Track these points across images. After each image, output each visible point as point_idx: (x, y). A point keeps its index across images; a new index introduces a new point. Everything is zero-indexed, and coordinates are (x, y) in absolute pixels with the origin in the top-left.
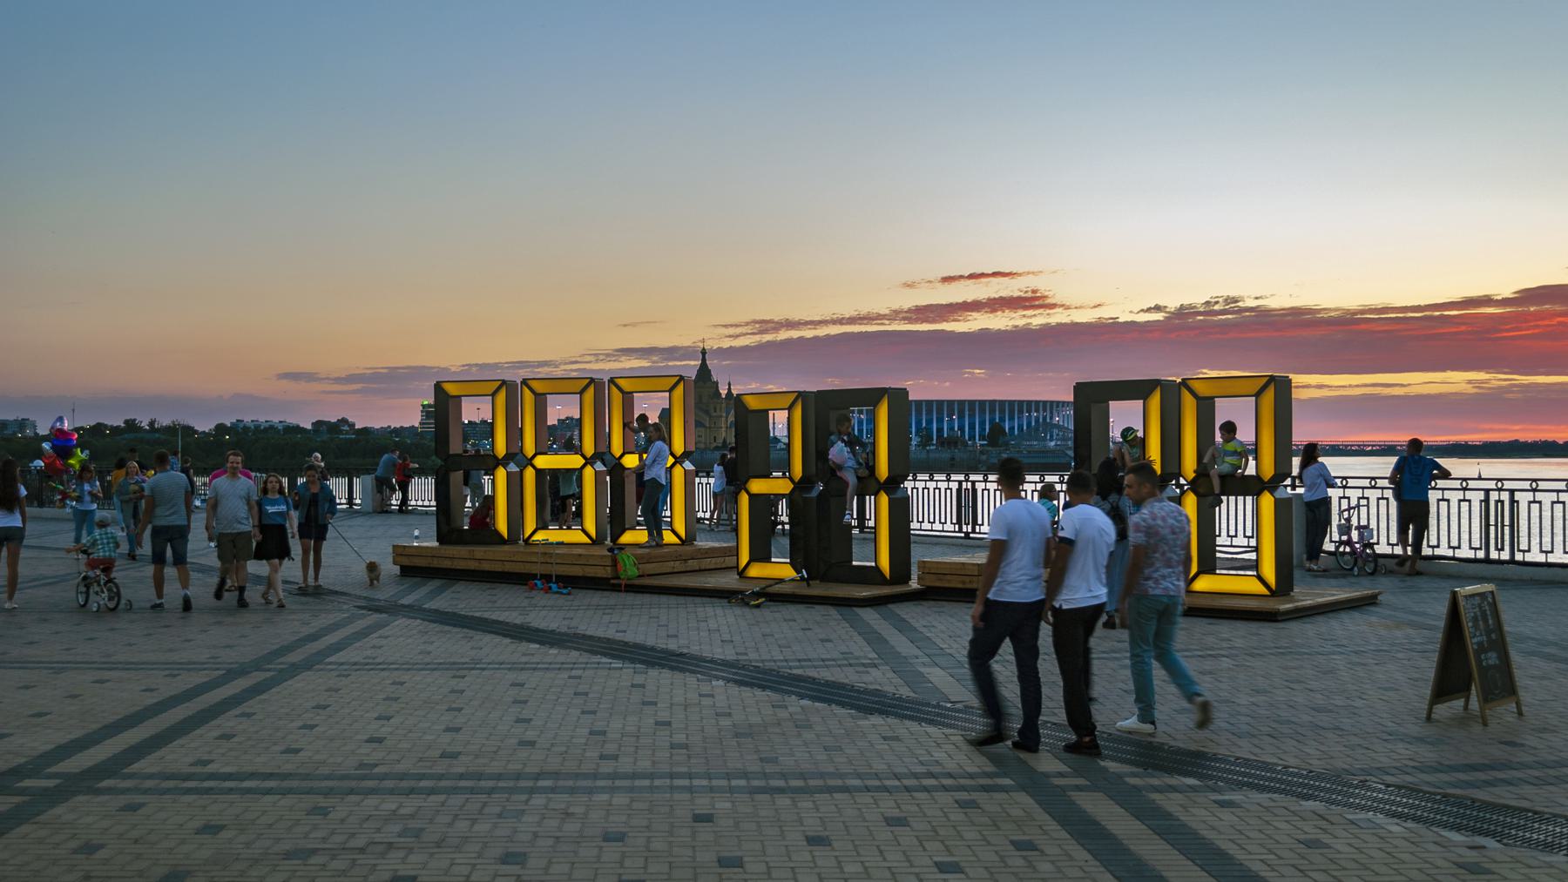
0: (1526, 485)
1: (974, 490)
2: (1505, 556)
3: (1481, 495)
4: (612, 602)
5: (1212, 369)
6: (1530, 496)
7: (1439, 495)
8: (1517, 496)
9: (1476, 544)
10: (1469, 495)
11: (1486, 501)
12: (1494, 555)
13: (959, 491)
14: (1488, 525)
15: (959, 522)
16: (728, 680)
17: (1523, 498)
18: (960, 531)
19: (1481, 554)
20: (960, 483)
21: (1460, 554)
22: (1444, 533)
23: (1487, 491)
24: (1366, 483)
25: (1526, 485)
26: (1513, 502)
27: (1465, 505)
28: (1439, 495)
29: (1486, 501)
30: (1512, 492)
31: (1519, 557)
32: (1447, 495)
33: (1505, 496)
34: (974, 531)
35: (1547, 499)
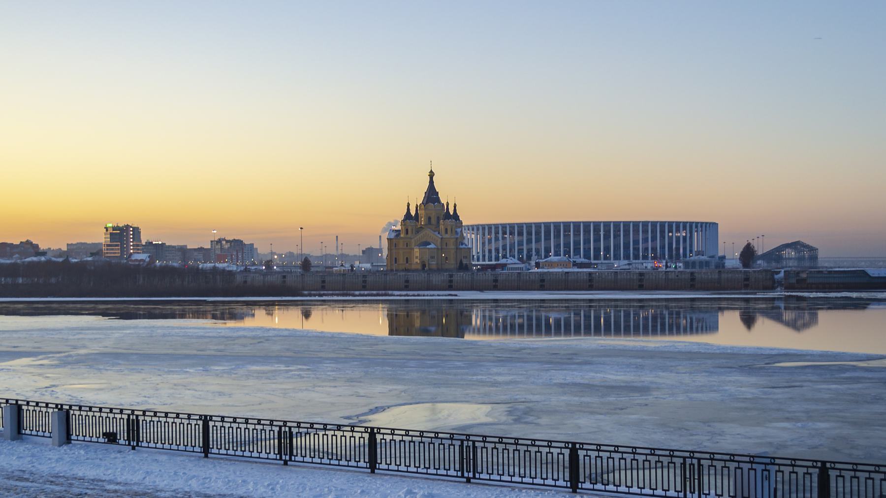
0: (707, 456)
3: (681, 460)
5: (33, 262)
9: (679, 489)
10: (674, 460)
11: (684, 464)
13: (128, 420)
14: (463, 459)
15: (280, 453)
18: (281, 459)
20: (129, 415)
21: (669, 494)
23: (684, 458)
24: (563, 445)
25: (707, 456)
27: (752, 472)
28: (584, 452)
29: (684, 464)
30: (699, 459)
32: (741, 465)
34: (290, 460)
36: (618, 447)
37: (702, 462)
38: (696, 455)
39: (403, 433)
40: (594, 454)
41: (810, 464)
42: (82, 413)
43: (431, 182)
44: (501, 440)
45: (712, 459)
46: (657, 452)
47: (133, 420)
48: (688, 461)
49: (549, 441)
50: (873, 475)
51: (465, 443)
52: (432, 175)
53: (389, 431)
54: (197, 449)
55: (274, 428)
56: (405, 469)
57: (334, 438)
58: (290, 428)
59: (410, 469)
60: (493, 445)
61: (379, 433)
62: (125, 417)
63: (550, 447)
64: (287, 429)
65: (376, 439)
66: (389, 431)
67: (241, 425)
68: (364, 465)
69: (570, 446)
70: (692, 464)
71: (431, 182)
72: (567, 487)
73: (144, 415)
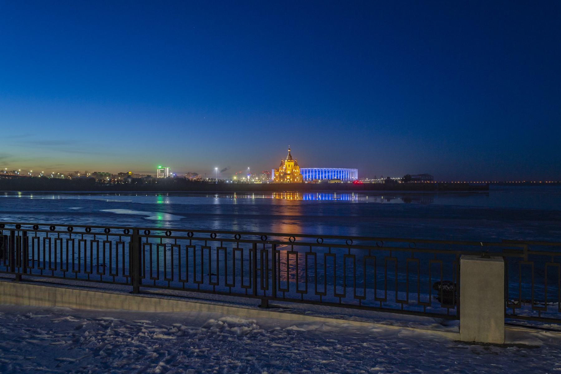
20: (13, 232)
39: (83, 230)
47: (19, 238)
64: (21, 234)
72: (127, 284)
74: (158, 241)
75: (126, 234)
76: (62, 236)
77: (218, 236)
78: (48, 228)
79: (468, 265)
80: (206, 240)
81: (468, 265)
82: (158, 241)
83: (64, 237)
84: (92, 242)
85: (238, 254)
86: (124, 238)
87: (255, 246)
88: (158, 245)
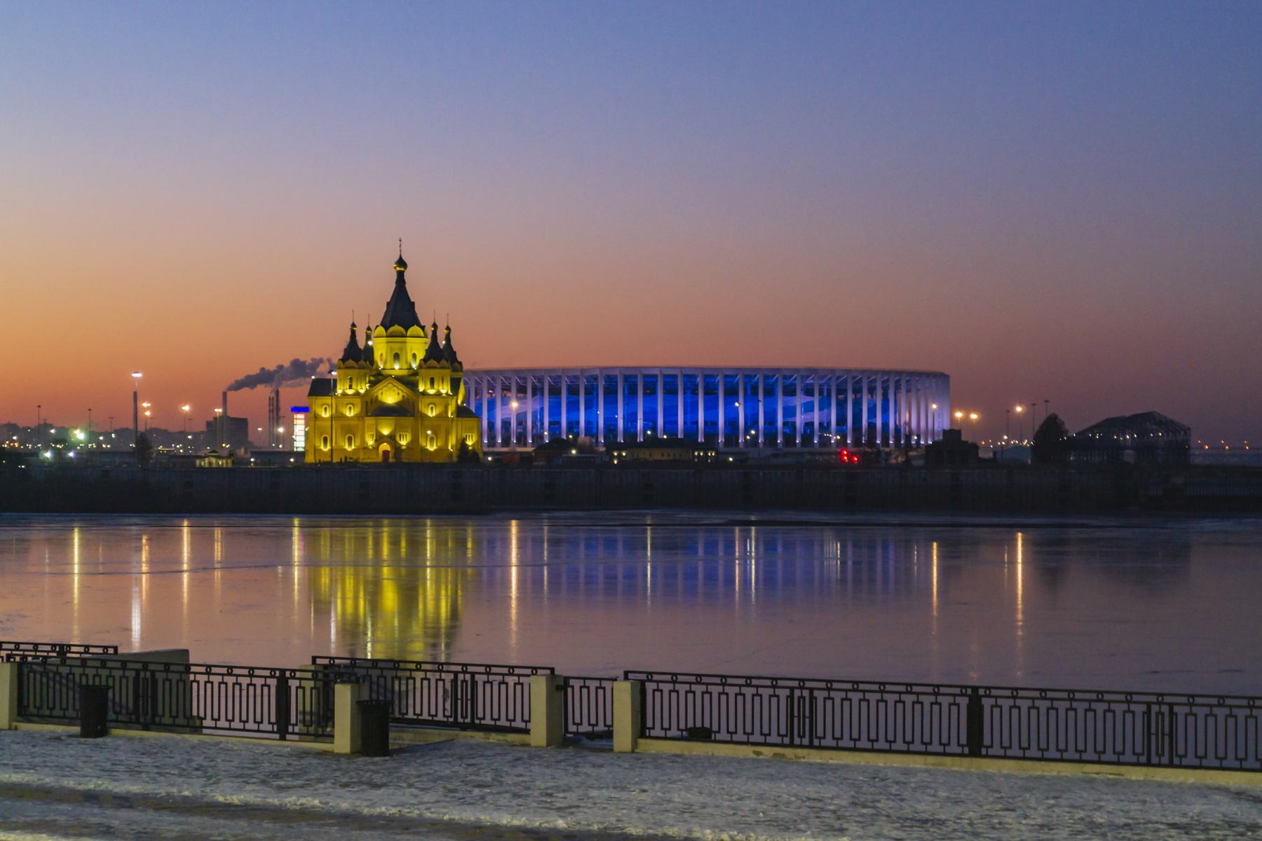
1: (155, 681)
2: (468, 720)
3: (1144, 708)
4: (561, 757)
6: (825, 694)
7: (654, 686)
8: (816, 693)
11: (791, 697)
12: (460, 720)
16: (757, 778)
17: (480, 679)
19: (451, 720)
20: (138, 672)
22: (749, 707)
24: (957, 691)
26: (812, 698)
28: (992, 701)
30: (1171, 705)
31: (477, 722)
32: (1000, 702)
33: (806, 693)
35: (891, 698)
36: (857, 683)
37: (1176, 709)
38: (808, 684)
39: (224, 671)
40: (245, 681)
41: (957, 691)
42: (171, 676)
43: (401, 276)
44: (1100, 695)
45: (1014, 698)
46: (1050, 695)
47: (145, 679)
48: (1155, 708)
49: (773, 679)
50: (904, 697)
51: (797, 693)
52: (401, 262)
53: (246, 672)
54: (265, 726)
55: (128, 673)
56: (226, 725)
57: (707, 697)
58: (153, 673)
59: (219, 724)
60: (219, 678)
61: (294, 678)
62: (131, 674)
63: (724, 685)
64: (148, 675)
65: (981, 708)
66: (203, 669)
67: (241, 680)
68: (269, 728)
69: (278, 674)
70: (1160, 713)
71: (401, 276)
72: (272, 732)
73: (167, 670)
74: (408, 674)
75: (272, 677)
76: (115, 673)
77: (298, 675)
78: (98, 664)
79: (338, 687)
80: (503, 675)
81: (338, 687)
82: (408, 674)
83: (245, 681)
84: (178, 682)
85: (382, 681)
86: (269, 681)
87: (456, 677)
88: (408, 679)
